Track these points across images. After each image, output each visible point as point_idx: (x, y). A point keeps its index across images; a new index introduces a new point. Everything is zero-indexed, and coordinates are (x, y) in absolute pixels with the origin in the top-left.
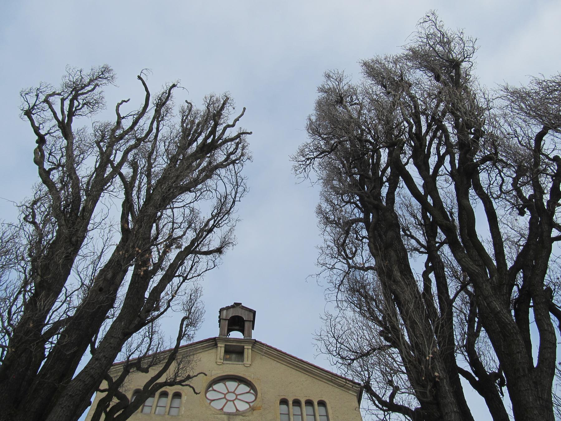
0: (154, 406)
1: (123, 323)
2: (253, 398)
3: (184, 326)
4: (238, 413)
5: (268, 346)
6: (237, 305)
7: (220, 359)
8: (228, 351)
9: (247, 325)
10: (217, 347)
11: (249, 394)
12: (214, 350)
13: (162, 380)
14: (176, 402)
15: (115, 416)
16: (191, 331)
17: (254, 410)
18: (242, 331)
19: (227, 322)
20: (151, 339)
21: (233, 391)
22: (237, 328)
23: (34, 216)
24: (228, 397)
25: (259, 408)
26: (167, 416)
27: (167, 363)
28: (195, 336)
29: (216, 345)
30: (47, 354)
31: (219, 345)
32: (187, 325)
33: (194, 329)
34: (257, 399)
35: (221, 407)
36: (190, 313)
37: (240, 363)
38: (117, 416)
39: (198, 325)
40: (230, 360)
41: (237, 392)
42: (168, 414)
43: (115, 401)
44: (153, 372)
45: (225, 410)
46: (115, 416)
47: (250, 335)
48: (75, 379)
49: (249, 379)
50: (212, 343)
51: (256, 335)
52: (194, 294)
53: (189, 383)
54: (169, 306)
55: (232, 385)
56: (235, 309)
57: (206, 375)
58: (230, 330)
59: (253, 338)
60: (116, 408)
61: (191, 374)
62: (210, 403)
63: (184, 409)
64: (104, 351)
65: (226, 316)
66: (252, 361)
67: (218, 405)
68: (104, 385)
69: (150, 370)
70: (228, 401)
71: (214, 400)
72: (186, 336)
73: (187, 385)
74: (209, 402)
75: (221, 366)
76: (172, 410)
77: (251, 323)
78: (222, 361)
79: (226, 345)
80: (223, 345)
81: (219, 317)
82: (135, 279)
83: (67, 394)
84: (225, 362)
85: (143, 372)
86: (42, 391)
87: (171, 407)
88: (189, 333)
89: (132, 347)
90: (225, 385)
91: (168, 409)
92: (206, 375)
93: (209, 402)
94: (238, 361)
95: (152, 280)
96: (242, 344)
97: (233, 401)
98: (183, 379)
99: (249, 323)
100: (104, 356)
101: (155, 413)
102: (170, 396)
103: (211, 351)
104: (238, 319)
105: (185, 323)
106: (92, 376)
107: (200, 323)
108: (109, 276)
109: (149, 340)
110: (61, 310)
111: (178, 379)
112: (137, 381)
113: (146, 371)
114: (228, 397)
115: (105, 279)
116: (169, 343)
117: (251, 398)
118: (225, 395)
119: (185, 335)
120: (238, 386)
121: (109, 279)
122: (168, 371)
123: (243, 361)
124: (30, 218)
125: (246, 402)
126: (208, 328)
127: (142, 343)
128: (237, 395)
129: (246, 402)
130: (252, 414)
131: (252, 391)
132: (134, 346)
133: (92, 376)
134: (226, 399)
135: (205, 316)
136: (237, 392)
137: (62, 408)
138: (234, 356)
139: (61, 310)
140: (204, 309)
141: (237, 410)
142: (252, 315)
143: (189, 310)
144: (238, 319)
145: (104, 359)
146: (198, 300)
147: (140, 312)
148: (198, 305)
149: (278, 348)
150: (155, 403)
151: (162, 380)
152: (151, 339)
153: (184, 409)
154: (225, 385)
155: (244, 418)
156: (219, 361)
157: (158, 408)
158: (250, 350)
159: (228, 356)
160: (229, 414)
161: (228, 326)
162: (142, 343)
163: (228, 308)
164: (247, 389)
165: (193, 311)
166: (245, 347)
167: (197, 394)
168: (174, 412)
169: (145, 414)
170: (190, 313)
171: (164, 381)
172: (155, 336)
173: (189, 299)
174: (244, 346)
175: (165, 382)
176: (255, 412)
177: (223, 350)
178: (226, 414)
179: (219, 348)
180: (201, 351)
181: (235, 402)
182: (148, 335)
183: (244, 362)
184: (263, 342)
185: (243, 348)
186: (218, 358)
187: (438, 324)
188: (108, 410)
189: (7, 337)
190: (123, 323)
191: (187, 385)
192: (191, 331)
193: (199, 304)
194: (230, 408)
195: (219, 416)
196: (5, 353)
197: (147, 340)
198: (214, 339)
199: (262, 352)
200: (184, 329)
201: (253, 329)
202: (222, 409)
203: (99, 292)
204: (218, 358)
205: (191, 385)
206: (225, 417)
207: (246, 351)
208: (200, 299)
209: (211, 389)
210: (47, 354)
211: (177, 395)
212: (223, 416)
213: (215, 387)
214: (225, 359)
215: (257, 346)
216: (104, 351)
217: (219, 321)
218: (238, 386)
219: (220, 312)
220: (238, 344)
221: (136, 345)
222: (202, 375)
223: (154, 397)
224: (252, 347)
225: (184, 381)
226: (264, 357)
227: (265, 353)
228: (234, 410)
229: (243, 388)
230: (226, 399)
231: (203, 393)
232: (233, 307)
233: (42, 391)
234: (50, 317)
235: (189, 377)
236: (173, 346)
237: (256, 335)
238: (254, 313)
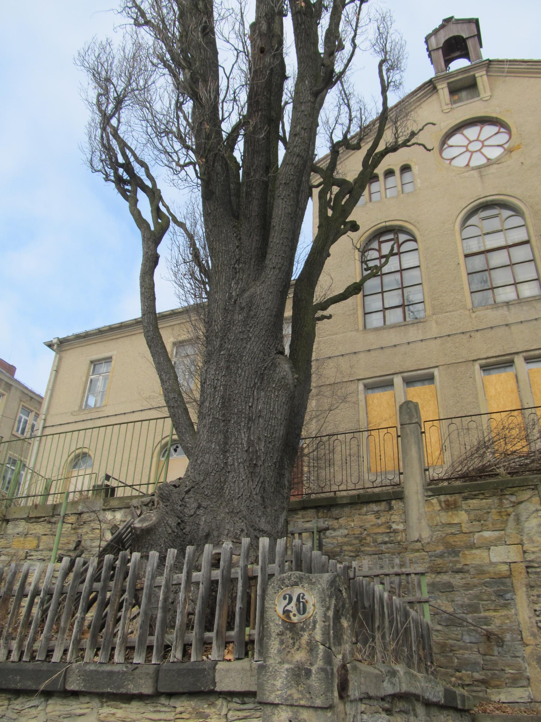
0: (383, 190)
1: (307, 82)
2: (505, 137)
3: (384, 73)
4: (490, 162)
5: (510, 61)
6: (448, 21)
7: (447, 104)
8: (454, 91)
9: (470, 44)
10: (437, 91)
11: (499, 135)
12: (435, 97)
13: (381, 147)
14: (407, 176)
15: (343, 203)
16: (395, 76)
17: (511, 152)
18: (466, 55)
19: (440, 52)
20: (349, 106)
21: (475, 138)
22: (457, 54)
23: (143, 14)
24: (471, 148)
25: (518, 147)
26: (402, 196)
27: (379, 127)
28: (403, 80)
29: (435, 89)
30: (241, 163)
31: (439, 87)
32: (388, 70)
33: (398, 72)
34: (512, 137)
35: (466, 163)
36: (386, 53)
37: (476, 99)
38: (345, 202)
39: (402, 65)
40: (460, 100)
41: (482, 138)
42: (403, 192)
43: (335, 189)
44: (366, 147)
45: (473, 164)
46: (343, 203)
47: (479, 56)
48: (281, 166)
49: (494, 115)
50: (430, 87)
51: (488, 52)
52: (382, 26)
53: (416, 141)
54: (355, 47)
55: (472, 132)
56: (446, 28)
57: (434, 124)
58: (448, 62)
59: (485, 58)
60: (339, 197)
61: (415, 129)
62: (450, 163)
63: (419, 181)
64: (300, 123)
65: (437, 44)
66: (491, 90)
67: (461, 162)
68: (316, 179)
69: (362, 145)
70: (472, 153)
71: (454, 158)
72: (392, 84)
73: (414, 144)
74: (448, 162)
75: (450, 114)
76: (405, 187)
77: (476, 38)
78: (450, 106)
79: (448, 84)
80: (445, 85)
81: (428, 49)
82: (297, 20)
83: (281, 184)
84: (454, 106)
85: (354, 149)
86: (254, 192)
87: (402, 185)
88: (393, 80)
89: (330, 122)
90: (463, 134)
91: (399, 188)
92: (434, 124)
93: (448, 162)
94: (472, 98)
95: (319, 26)
96: (472, 73)
97: (479, 150)
98: (407, 137)
99: (472, 39)
100: (302, 128)
101: (386, 197)
102: (397, 172)
103: (430, 100)
104: (455, 42)
105: (384, 68)
106: (298, 155)
107: (404, 61)
108: (264, 27)
109: (346, 109)
110: (231, 115)
111: (400, 141)
112: (351, 167)
113: (358, 147)
114: (471, 148)
115: (261, 35)
116: (373, 110)
117: (503, 138)
118: (466, 147)
119: (389, 83)
120: (481, 130)
121: (265, 32)
122: (384, 136)
123: (479, 96)
124: (141, 20)
125: (498, 146)
126: (418, 69)
127: (339, 114)
128: (483, 142)
129: (498, 146)
130: (510, 157)
131: (502, 130)
132: (332, 121)
133: (298, 155)
134: (470, 151)
135: (407, 49)
136: (482, 138)
137: (283, 199)
138: (464, 94)
139: (231, 115)
140: (403, 38)
141: (488, 159)
142: (474, 26)
143: (384, 50)
144: (455, 42)
145: (303, 132)
146: (391, 31)
147: (321, 76)
148: (393, 37)
149: (526, 58)
150: (383, 187)
151: (381, 147)
152: (349, 106)
153: (419, 181)
154: (463, 134)
155: (500, 165)
156: (445, 107)
157: (388, 191)
158: (485, 78)
159: (456, 97)
160: (479, 168)
161: (444, 56)
162: (339, 114)
163: (436, 32)
164: (494, 129)
165: (388, 49)
166: (477, 75)
167: (430, 150)
168: (408, 188)
169: (375, 202)
170: (386, 53)
171: (384, 147)
172: (352, 102)
173: (377, 35)
174: (474, 75)
175: (386, 149)
176: (513, 153)
177: (446, 91)
178: (473, 169)
179: (440, 92)
180: (418, 103)
181: (483, 150)
182: (341, 102)
183: (481, 96)
184: (501, 58)
185: (474, 78)
186: (443, 104)
187: (397, 631)
188: (332, 204)
189: (190, 153)
190: (307, 82)
191: (414, 144)
192: (395, 76)
193: (393, 37)
194: (478, 160)
195: (467, 174)
196: (197, 167)
197: (344, 109)
198: (431, 82)
199: (503, 72)
200: (385, 78)
201: (481, 46)
202: (468, 165)
203: (262, 55)
204: (443, 104)
205: (419, 142)
206: (475, 173)
207: (479, 80)
208: (393, 29)
209: (446, 146)
210: (241, 163)
211: (406, 168)
212: (472, 172)
213: (451, 141)
214: (453, 102)
215: (494, 67)
216: (300, 123)
217: (430, 56)
218: (481, 130)
219: (426, 42)
220: (465, 75)
221: (333, 119)
222: (430, 126)
223: (378, 181)
224: (487, 71)
225: (408, 140)
226: (507, 78)
227: (508, 72)
228: (484, 161)
229: (489, 130)
230: (470, 151)
231: (436, 150)
232: (442, 27)
233: (254, 192)
234: (222, 109)
235: (413, 134)
236: (380, 110)
237: (488, 52)
238: (476, 22)
